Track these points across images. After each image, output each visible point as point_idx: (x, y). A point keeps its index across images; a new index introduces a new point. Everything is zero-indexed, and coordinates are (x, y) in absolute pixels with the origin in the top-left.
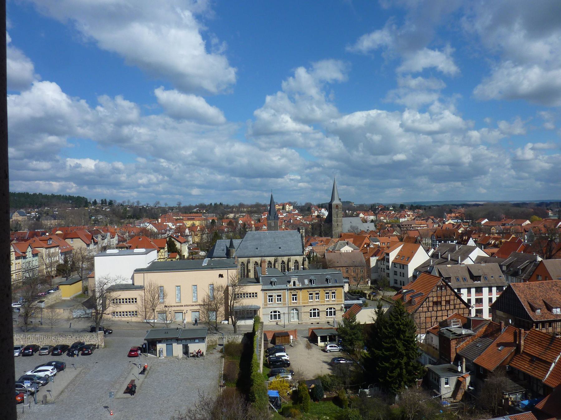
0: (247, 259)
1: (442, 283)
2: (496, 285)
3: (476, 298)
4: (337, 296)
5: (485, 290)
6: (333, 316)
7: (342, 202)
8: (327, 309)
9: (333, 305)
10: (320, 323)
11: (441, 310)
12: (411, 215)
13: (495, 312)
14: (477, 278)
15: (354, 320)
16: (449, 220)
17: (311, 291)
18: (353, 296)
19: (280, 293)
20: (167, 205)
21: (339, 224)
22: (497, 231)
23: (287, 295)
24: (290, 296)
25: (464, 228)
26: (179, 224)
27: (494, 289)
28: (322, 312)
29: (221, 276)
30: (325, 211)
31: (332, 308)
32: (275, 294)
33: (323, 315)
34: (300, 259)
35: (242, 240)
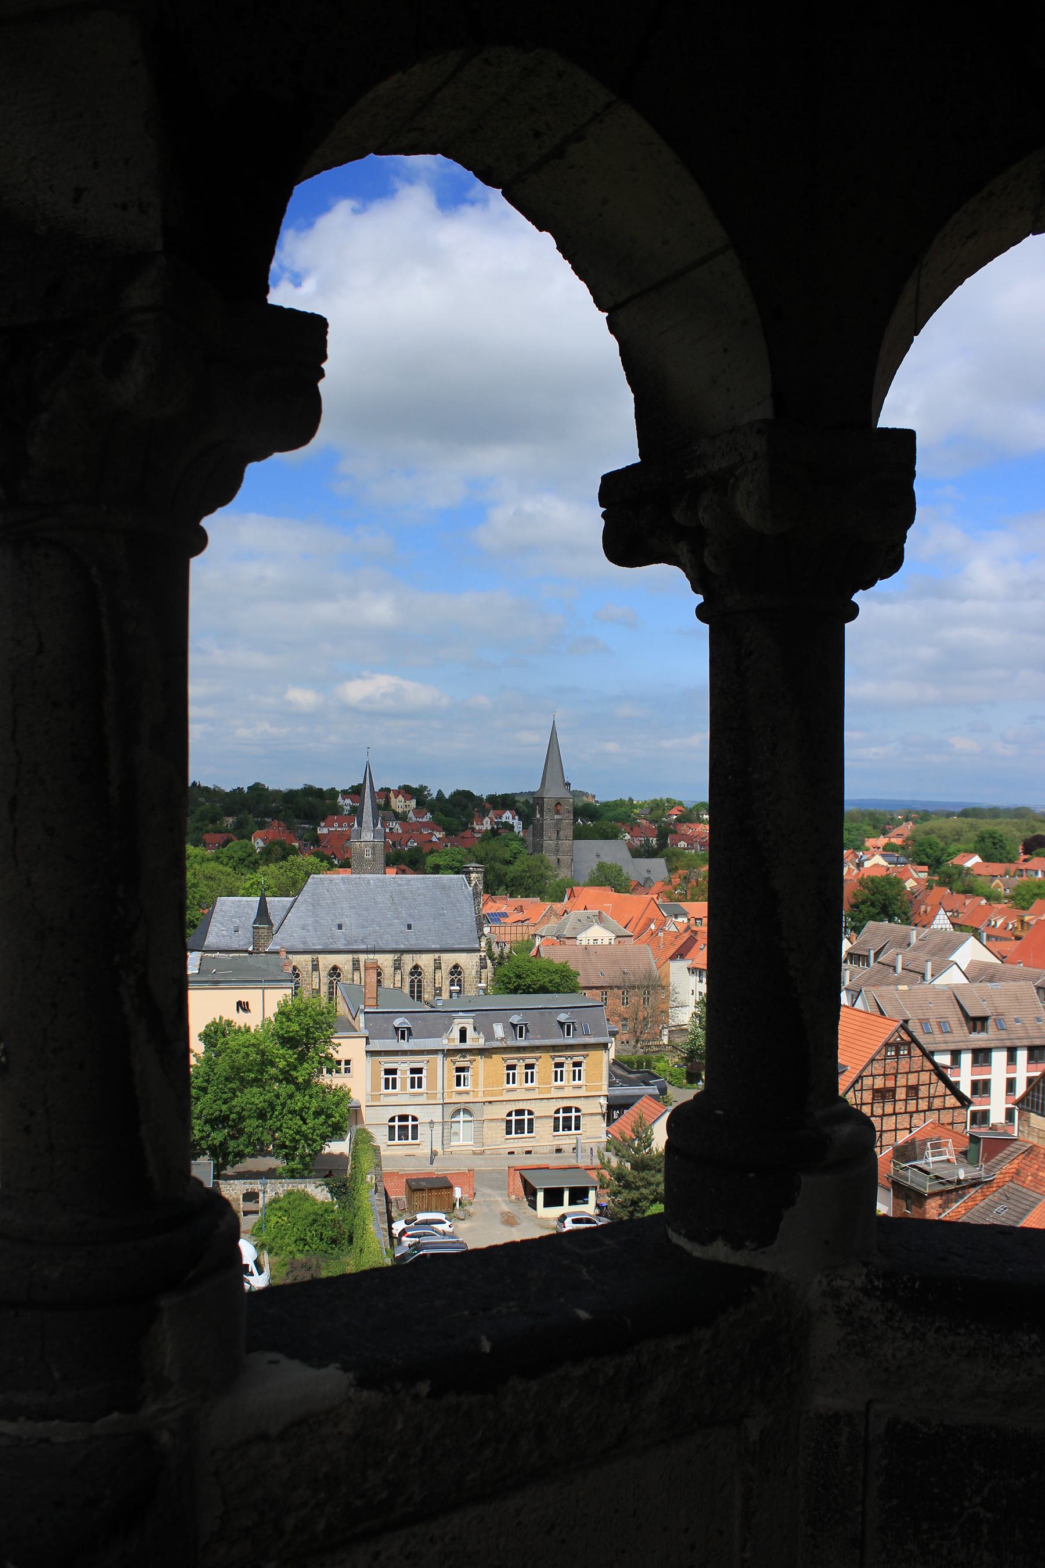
0: (308, 957)
1: (900, 1037)
2: (1027, 1043)
3: (1007, 1079)
4: (587, 1074)
5: (999, 1058)
6: (573, 1131)
9: (576, 1100)
10: (536, 1153)
11: (895, 1114)
13: (1028, 1121)
14: (977, 1023)
16: (873, 855)
17: (512, 1058)
18: (630, 1072)
19: (417, 1061)
21: (564, 858)
22: (1008, 891)
23: (441, 1069)
24: (450, 1071)
25: (915, 880)
27: (1022, 1055)
29: (243, 1007)
30: (514, 818)
31: (571, 1108)
32: (403, 1066)
33: (544, 1129)
35: (295, 901)
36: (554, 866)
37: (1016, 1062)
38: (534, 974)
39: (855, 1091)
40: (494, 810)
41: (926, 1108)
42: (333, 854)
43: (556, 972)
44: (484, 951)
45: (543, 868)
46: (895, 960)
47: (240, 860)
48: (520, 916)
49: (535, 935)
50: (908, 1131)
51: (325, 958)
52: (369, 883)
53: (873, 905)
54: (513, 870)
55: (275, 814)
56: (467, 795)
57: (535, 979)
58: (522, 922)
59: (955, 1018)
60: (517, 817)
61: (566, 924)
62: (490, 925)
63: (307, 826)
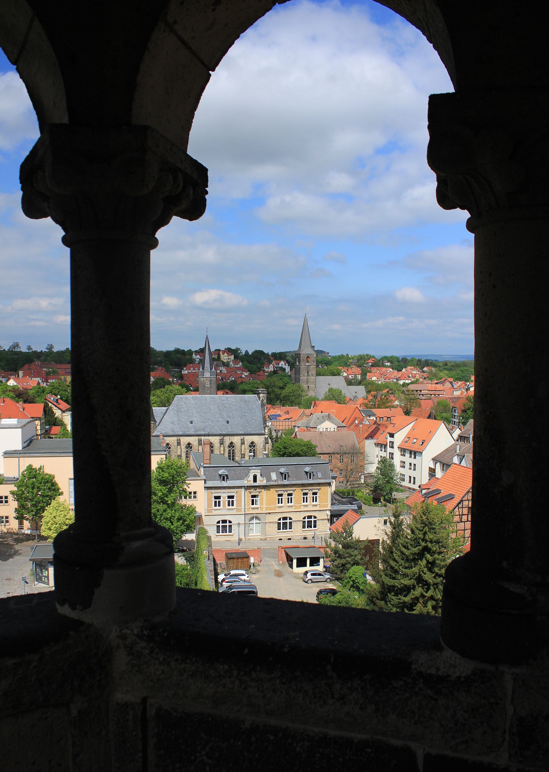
0: (175, 439)
4: (320, 499)
6: (313, 528)
7: (315, 351)
8: (304, 518)
12: (417, 375)
15: (351, 534)
17: (281, 491)
18: (343, 498)
19: (231, 492)
20: (32, 349)
21: (311, 386)
23: (243, 496)
26: (51, 381)
28: (321, 521)
30: (285, 365)
31: (311, 516)
32: (224, 495)
34: (259, 440)
39: (459, 508)
40: (275, 360)
43: (304, 445)
48: (287, 416)
51: (184, 439)
54: (285, 392)
56: (261, 353)
58: (289, 419)
60: (287, 364)
61: (311, 420)
62: (271, 421)
63: (177, 370)
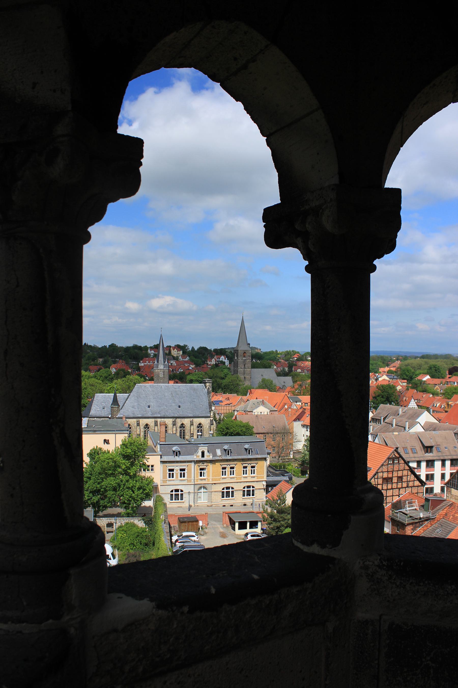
0: (135, 420)
1: (395, 455)
2: (450, 457)
3: (442, 473)
4: (257, 471)
5: (438, 464)
6: (251, 496)
9: (252, 483)
10: (235, 506)
11: (392, 489)
13: (450, 492)
14: (428, 449)
16: (383, 375)
17: (224, 464)
19: (183, 466)
21: (247, 377)
22: (442, 391)
23: (193, 469)
25: (401, 386)
27: (448, 463)
30: (225, 359)
31: (250, 486)
32: (177, 468)
33: (238, 495)
35: (129, 395)
36: (243, 380)
37: (445, 466)
38: (234, 427)
39: (375, 479)
40: (216, 355)
41: (406, 486)
42: (146, 375)
43: (244, 427)
44: (212, 417)
45: (238, 381)
46: (392, 421)
47: (105, 377)
48: (228, 402)
49: (234, 410)
50: (398, 496)
51: (142, 420)
52: (162, 387)
53: (382, 397)
55: (120, 357)
56: (205, 349)
57: (235, 430)
58: (229, 404)
59: (418, 447)
60: (226, 359)
61: (248, 405)
62: (215, 406)
63: (135, 362)
